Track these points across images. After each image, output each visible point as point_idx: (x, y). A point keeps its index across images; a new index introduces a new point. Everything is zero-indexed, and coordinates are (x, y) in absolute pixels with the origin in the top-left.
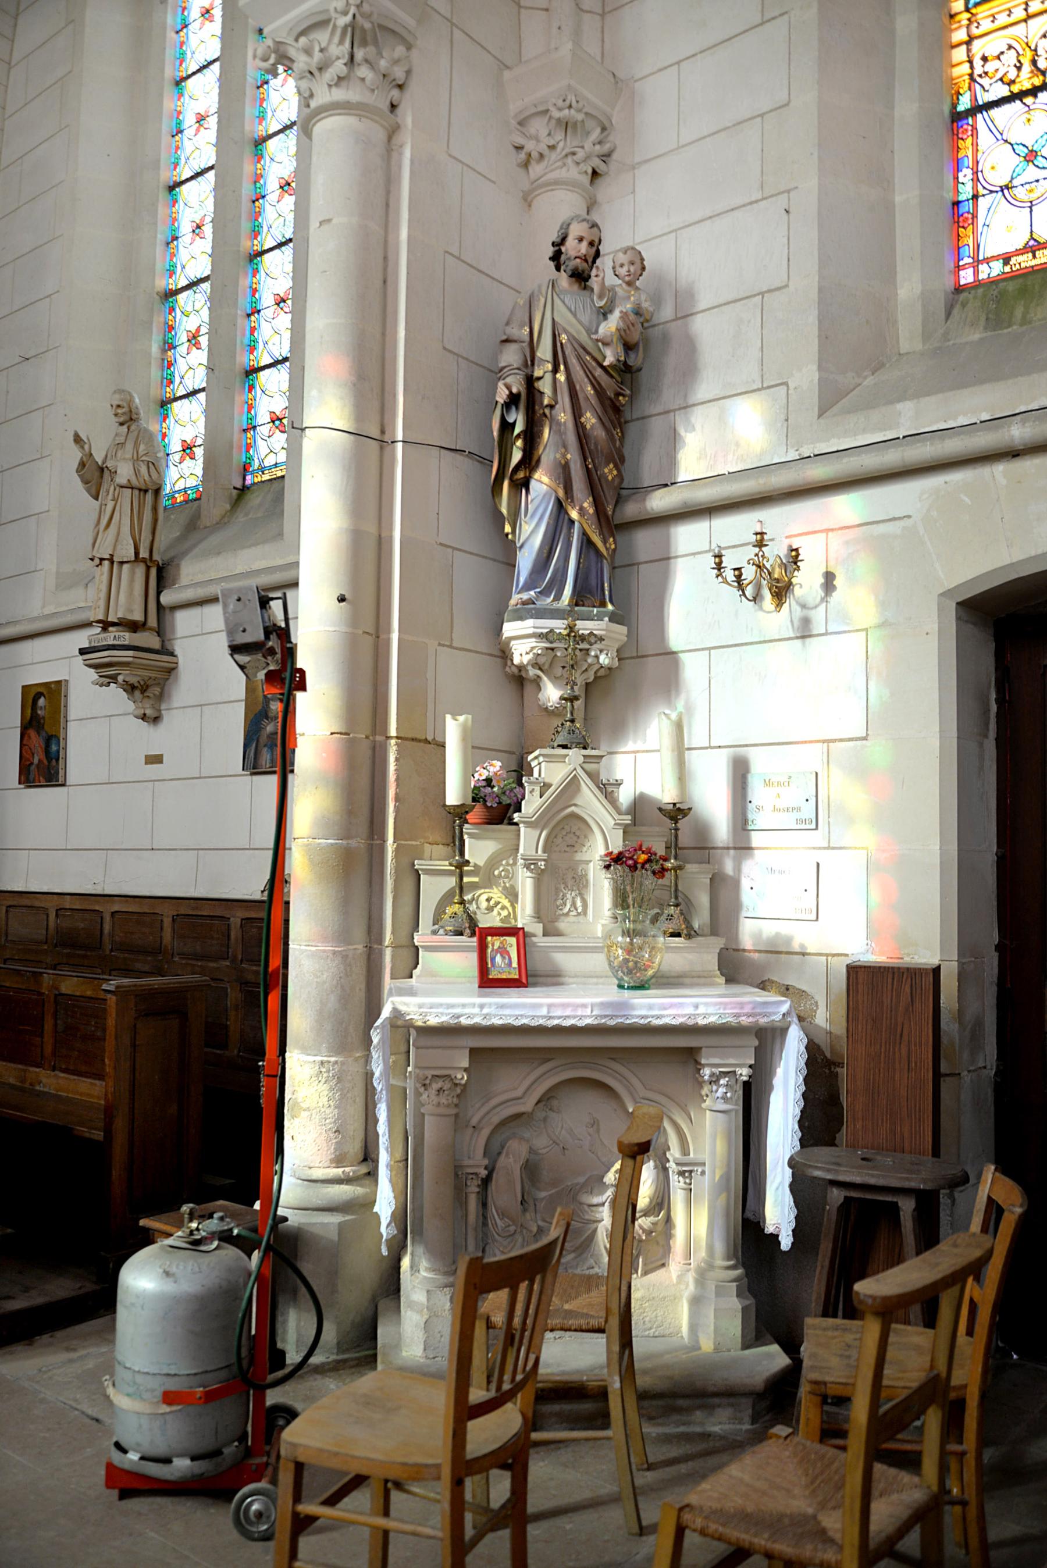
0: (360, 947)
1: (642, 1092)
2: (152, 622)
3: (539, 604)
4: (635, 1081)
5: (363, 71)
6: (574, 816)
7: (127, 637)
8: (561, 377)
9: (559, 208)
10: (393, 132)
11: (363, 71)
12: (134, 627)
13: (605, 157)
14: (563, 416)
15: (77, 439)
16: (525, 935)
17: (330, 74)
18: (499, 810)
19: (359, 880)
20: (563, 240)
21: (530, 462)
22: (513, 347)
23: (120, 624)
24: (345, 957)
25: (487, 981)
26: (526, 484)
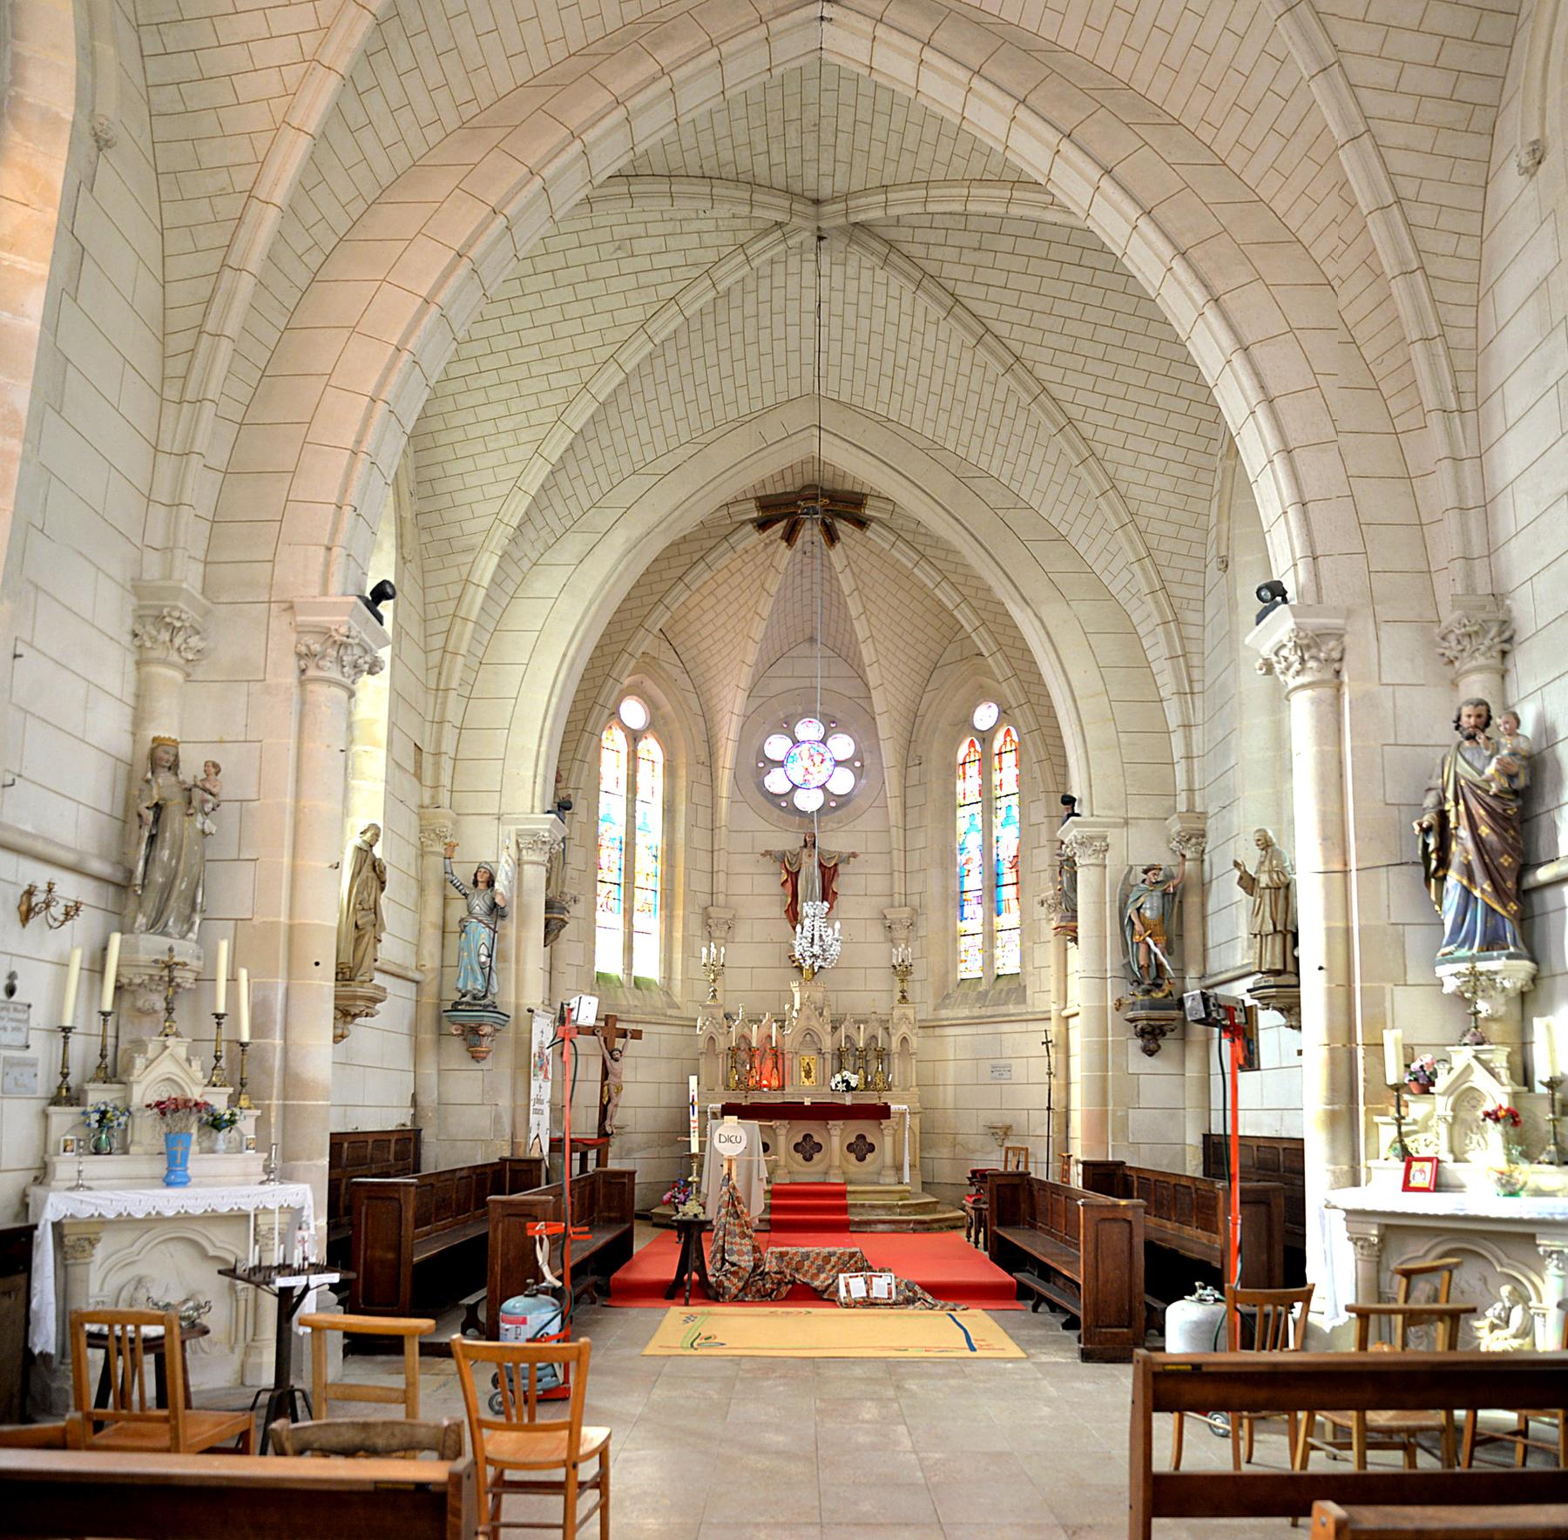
0: (1345, 1168)
1: (1505, 1260)
2: (1290, 967)
3: (1457, 954)
4: (1499, 1252)
5: (1312, 664)
6: (1472, 1088)
7: (1272, 980)
8: (1462, 808)
9: (1476, 686)
10: (1339, 688)
11: (1312, 664)
12: (1277, 973)
13: (1510, 640)
14: (1464, 833)
15: (1236, 864)
16: (1439, 1161)
17: (1292, 671)
18: (1425, 1083)
19: (1343, 1131)
20: (1459, 718)
21: (1444, 863)
22: (1433, 793)
23: (1270, 972)
24: (1334, 1172)
25: (1407, 1187)
26: (1444, 878)
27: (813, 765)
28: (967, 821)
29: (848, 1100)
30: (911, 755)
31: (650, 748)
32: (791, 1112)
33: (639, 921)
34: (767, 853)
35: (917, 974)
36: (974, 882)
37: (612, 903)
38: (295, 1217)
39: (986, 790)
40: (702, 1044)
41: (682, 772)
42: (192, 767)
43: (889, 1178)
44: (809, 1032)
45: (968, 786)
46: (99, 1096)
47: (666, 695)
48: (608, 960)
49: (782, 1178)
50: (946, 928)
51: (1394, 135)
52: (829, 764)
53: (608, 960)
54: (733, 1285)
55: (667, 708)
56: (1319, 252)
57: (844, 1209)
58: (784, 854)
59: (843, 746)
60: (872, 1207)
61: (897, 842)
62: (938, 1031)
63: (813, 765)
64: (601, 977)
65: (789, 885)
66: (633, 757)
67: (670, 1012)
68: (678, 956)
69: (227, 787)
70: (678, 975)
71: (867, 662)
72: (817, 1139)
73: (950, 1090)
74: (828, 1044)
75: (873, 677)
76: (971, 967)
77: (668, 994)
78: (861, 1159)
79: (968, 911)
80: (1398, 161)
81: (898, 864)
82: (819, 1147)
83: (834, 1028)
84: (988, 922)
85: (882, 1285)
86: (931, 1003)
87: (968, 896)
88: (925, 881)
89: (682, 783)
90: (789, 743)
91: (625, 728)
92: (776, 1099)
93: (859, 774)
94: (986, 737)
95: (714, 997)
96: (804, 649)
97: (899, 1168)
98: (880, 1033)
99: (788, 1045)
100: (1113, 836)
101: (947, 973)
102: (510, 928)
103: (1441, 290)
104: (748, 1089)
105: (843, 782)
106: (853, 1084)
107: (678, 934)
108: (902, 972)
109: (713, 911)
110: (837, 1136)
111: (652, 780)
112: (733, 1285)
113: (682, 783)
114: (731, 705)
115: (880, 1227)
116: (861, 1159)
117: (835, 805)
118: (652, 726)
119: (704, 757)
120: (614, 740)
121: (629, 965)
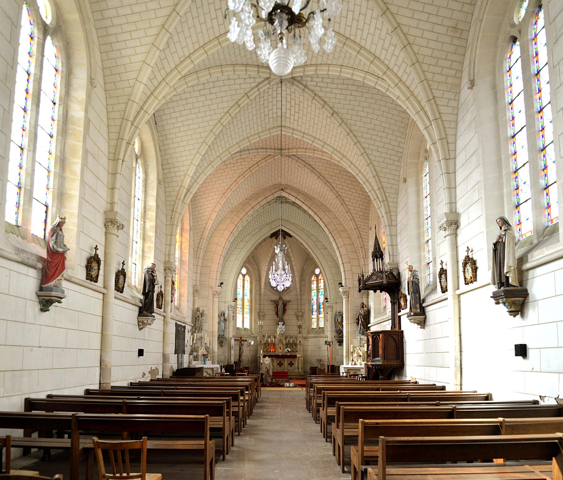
28: (314, 293)
29: (288, 354)
31: (247, 278)
32: (277, 357)
34: (272, 301)
35: (303, 327)
36: (315, 307)
38: (218, 368)
39: (317, 287)
40: (259, 342)
42: (201, 311)
43: (296, 371)
44: (280, 340)
45: (314, 286)
46: (195, 354)
48: (239, 325)
49: (275, 370)
51: (356, 219)
53: (239, 325)
54: (268, 384)
55: (251, 269)
56: (349, 232)
57: (287, 376)
61: (299, 298)
64: (238, 328)
66: (244, 280)
68: (253, 323)
69: (205, 313)
70: (253, 327)
74: (284, 342)
76: (314, 326)
77: (251, 331)
78: (291, 366)
79: (314, 313)
80: (357, 223)
81: (299, 303)
82: (282, 364)
83: (286, 339)
84: (318, 316)
85: (292, 385)
89: (254, 285)
91: (242, 274)
92: (274, 354)
94: (317, 276)
97: (299, 368)
99: (276, 343)
100: (334, 306)
102: (227, 323)
103: (363, 240)
104: (268, 352)
107: (253, 318)
108: (300, 327)
109: (260, 313)
110: (286, 362)
112: (268, 384)
113: (254, 285)
116: (291, 366)
117: (287, 290)
118: (247, 273)
119: (258, 279)
121: (243, 325)
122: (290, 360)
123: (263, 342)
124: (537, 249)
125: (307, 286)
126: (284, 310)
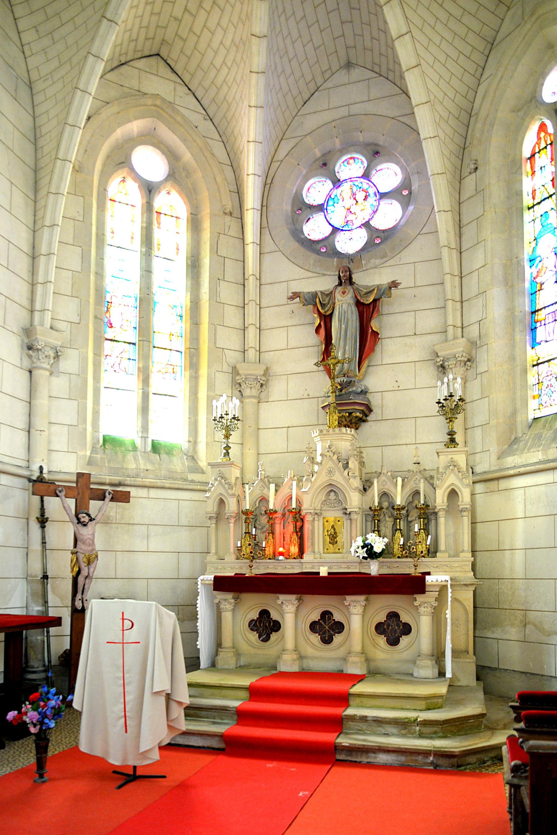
27: (353, 204)
29: (374, 568)
30: (464, 162)
33: (156, 383)
34: (296, 295)
37: (125, 363)
41: (206, 225)
44: (332, 489)
47: (184, 141)
50: (512, 358)
52: (372, 199)
55: (187, 156)
58: (315, 295)
59: (389, 176)
60: (379, 721)
62: (503, 484)
63: (353, 204)
65: (322, 331)
67: (191, 477)
71: (394, 34)
72: (337, 617)
73: (519, 556)
75: (417, 93)
77: (193, 458)
86: (494, 449)
87: (540, 316)
88: (485, 306)
90: (329, 185)
91: (137, 178)
93: (406, 202)
95: (227, 454)
96: (342, 77)
98: (422, 486)
101: (514, 414)
105: (389, 215)
106: (378, 548)
108: (451, 408)
110: (358, 615)
111: (172, 235)
113: (206, 235)
114: (251, 131)
115: (382, 758)
116: (394, 642)
120: (124, 193)
121: (145, 428)
122: (382, 606)
123: (232, 506)
124: (203, 705)
125: (496, 191)
126: (367, 340)
